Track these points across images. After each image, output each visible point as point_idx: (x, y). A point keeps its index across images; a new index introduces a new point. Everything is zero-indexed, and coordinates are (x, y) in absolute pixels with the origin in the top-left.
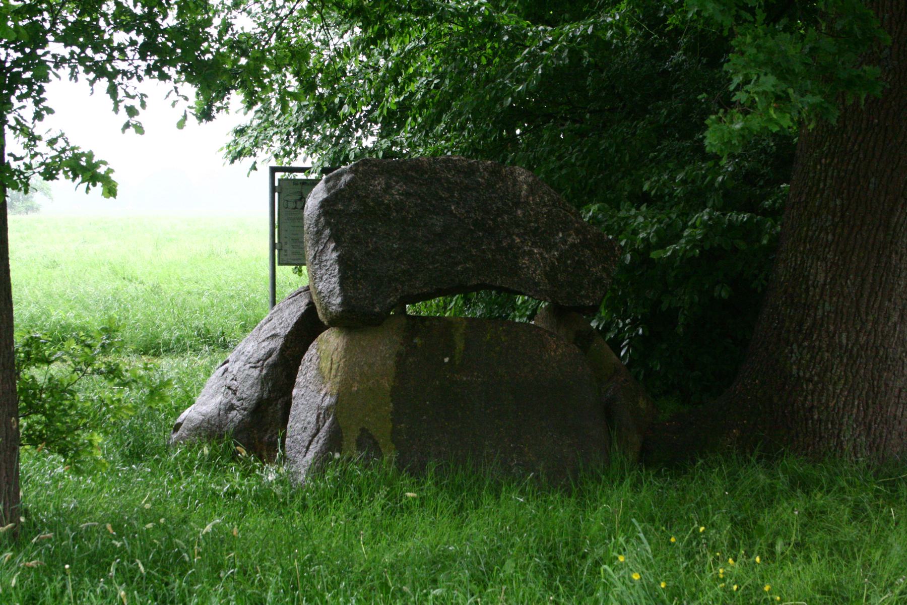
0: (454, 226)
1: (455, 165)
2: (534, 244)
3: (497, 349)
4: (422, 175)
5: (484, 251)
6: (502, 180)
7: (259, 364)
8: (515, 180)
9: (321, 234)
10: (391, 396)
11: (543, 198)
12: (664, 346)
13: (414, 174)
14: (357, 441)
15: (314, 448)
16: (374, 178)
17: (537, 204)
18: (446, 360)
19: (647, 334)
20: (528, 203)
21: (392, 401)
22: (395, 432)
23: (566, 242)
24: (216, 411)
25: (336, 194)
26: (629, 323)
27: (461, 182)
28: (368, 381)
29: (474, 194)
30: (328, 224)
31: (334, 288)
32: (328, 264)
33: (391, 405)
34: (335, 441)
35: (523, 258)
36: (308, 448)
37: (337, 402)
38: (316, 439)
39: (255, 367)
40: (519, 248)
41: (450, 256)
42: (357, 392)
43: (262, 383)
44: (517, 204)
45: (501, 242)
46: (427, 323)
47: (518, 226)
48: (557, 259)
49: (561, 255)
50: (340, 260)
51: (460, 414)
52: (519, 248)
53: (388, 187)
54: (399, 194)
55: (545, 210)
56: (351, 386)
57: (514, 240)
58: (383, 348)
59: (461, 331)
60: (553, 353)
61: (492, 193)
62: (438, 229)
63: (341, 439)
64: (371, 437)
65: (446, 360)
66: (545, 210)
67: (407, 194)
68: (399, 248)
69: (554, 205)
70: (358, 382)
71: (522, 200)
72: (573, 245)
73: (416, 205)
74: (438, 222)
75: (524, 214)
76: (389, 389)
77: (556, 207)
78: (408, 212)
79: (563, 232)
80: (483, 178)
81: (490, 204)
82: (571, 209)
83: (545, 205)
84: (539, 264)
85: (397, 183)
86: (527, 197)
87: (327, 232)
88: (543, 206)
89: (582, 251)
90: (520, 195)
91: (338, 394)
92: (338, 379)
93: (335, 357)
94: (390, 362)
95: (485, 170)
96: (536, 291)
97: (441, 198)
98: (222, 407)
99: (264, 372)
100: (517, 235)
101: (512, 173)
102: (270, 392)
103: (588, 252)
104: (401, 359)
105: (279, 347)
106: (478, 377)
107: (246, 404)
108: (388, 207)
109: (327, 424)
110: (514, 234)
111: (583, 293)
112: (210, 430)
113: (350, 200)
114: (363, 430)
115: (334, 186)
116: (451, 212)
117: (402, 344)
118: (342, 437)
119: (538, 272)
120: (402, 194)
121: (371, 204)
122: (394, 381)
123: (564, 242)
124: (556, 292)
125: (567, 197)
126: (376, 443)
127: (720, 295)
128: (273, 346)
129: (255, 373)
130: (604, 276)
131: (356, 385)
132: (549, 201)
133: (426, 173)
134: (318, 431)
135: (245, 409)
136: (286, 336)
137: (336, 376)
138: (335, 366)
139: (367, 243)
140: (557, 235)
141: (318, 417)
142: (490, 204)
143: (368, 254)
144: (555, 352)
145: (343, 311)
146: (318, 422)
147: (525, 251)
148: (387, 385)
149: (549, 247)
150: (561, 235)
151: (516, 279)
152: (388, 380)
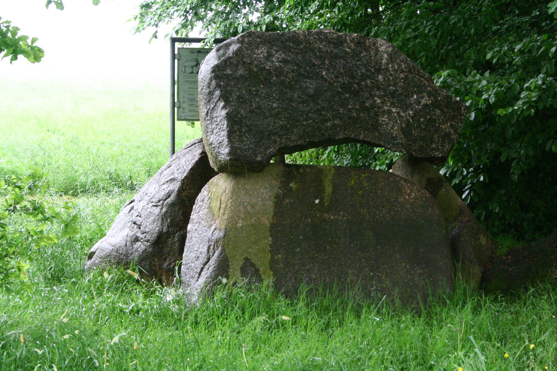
0: (325, 88)
1: (327, 37)
2: (393, 105)
3: (360, 192)
4: (298, 45)
5: (349, 110)
6: (365, 50)
7: (160, 204)
8: (377, 50)
9: (213, 94)
10: (270, 231)
11: (400, 65)
12: (503, 192)
13: (291, 45)
14: (241, 269)
15: (206, 274)
16: (257, 48)
17: (395, 71)
18: (317, 201)
19: (487, 181)
20: (387, 70)
21: (271, 236)
22: (273, 263)
23: (420, 103)
24: (124, 243)
25: (225, 61)
26: (472, 172)
27: (331, 52)
28: (251, 219)
29: (342, 62)
30: (218, 86)
31: (223, 140)
32: (219, 119)
33: (270, 239)
34: (223, 268)
35: (383, 116)
36: (200, 274)
37: (225, 236)
38: (207, 266)
39: (156, 206)
40: (379, 108)
41: (321, 114)
42: (242, 228)
43: (162, 219)
44: (378, 71)
45: (364, 102)
46: (301, 170)
47: (379, 89)
48: (412, 117)
49: (415, 114)
50: (229, 117)
51: (328, 247)
52: (379, 108)
53: (269, 56)
54: (279, 61)
55: (402, 75)
56: (237, 223)
57: (375, 101)
58: (263, 192)
59: (330, 178)
60: (407, 197)
61: (358, 61)
62: (311, 92)
63: (228, 266)
64: (253, 265)
65: (317, 201)
66: (402, 75)
67: (285, 61)
68: (277, 107)
69: (409, 71)
70: (243, 220)
71: (383, 67)
72: (426, 105)
73: (293, 71)
74: (311, 85)
75: (384, 79)
76: (268, 225)
77: (412, 73)
78: (285, 77)
79: (417, 94)
80: (350, 48)
81: (356, 71)
82: (424, 75)
83: (402, 71)
84: (396, 122)
85: (277, 52)
86: (387, 64)
87: (218, 93)
88: (401, 73)
89: (434, 110)
90: (381, 63)
91: (226, 229)
92: (226, 217)
93: (223, 198)
94: (270, 204)
95: (351, 41)
96: (394, 144)
97: (314, 65)
98: (129, 239)
99: (164, 210)
100: (378, 97)
101: (374, 44)
102: (168, 227)
103: (438, 112)
104: (278, 201)
105: (177, 189)
106: (343, 216)
107: (148, 237)
108: (269, 72)
109: (216, 254)
110: (375, 95)
111: (434, 146)
112: (120, 259)
113: (237, 66)
114: (246, 259)
115: (224, 54)
116: (323, 76)
117: (280, 188)
118: (228, 265)
119: (396, 128)
120: (281, 62)
121: (255, 69)
122: (273, 219)
123: (418, 102)
124: (410, 145)
125: (422, 64)
126: (257, 271)
127: (551, 149)
128: (172, 188)
129: (157, 210)
130: (452, 131)
131: (241, 221)
132: (405, 68)
133: (302, 43)
134: (209, 259)
135: (148, 241)
136: (183, 180)
137: (224, 214)
138: (223, 206)
139: (251, 103)
140: (413, 96)
141: (209, 248)
142: (356, 71)
143: (252, 112)
144: (409, 196)
145: (230, 160)
146: (208, 252)
147: (384, 110)
148: (266, 221)
149: (406, 107)
150: (415, 97)
151: (377, 134)
152: (268, 218)
